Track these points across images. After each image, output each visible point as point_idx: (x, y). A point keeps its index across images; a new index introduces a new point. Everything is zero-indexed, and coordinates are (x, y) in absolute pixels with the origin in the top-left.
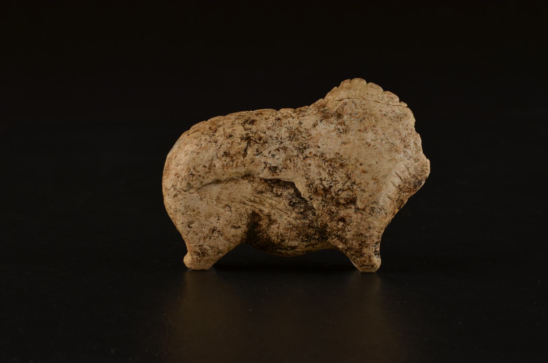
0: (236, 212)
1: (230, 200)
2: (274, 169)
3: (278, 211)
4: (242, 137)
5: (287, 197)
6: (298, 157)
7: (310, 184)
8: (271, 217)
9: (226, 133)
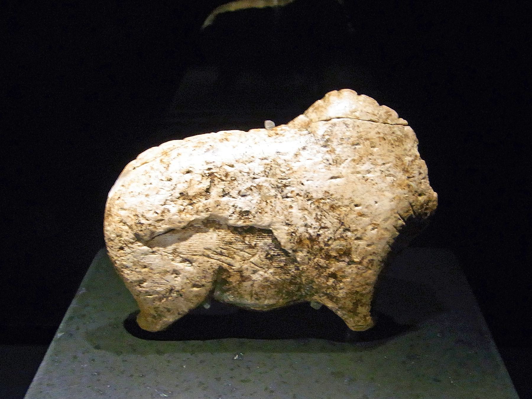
3: (252, 265)
7: (293, 232)
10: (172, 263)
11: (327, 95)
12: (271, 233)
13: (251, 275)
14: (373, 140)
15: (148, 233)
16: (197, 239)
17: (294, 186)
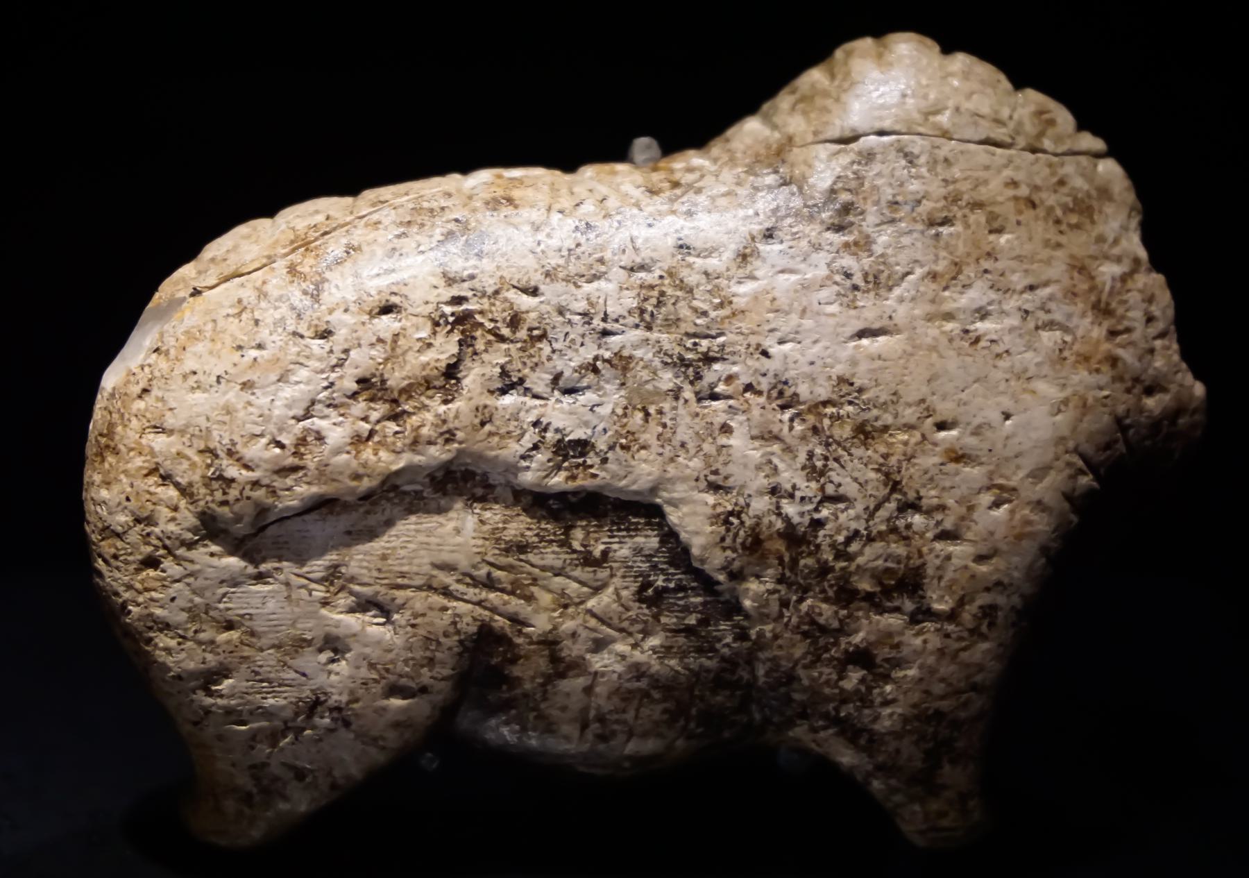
0: (409, 629)
1: (386, 581)
3: (593, 622)
4: (436, 316)
5: (628, 567)
6: (677, 398)
7: (731, 513)
8: (561, 650)
10: (324, 612)
13: (588, 656)
14: (997, 209)
17: (736, 358)
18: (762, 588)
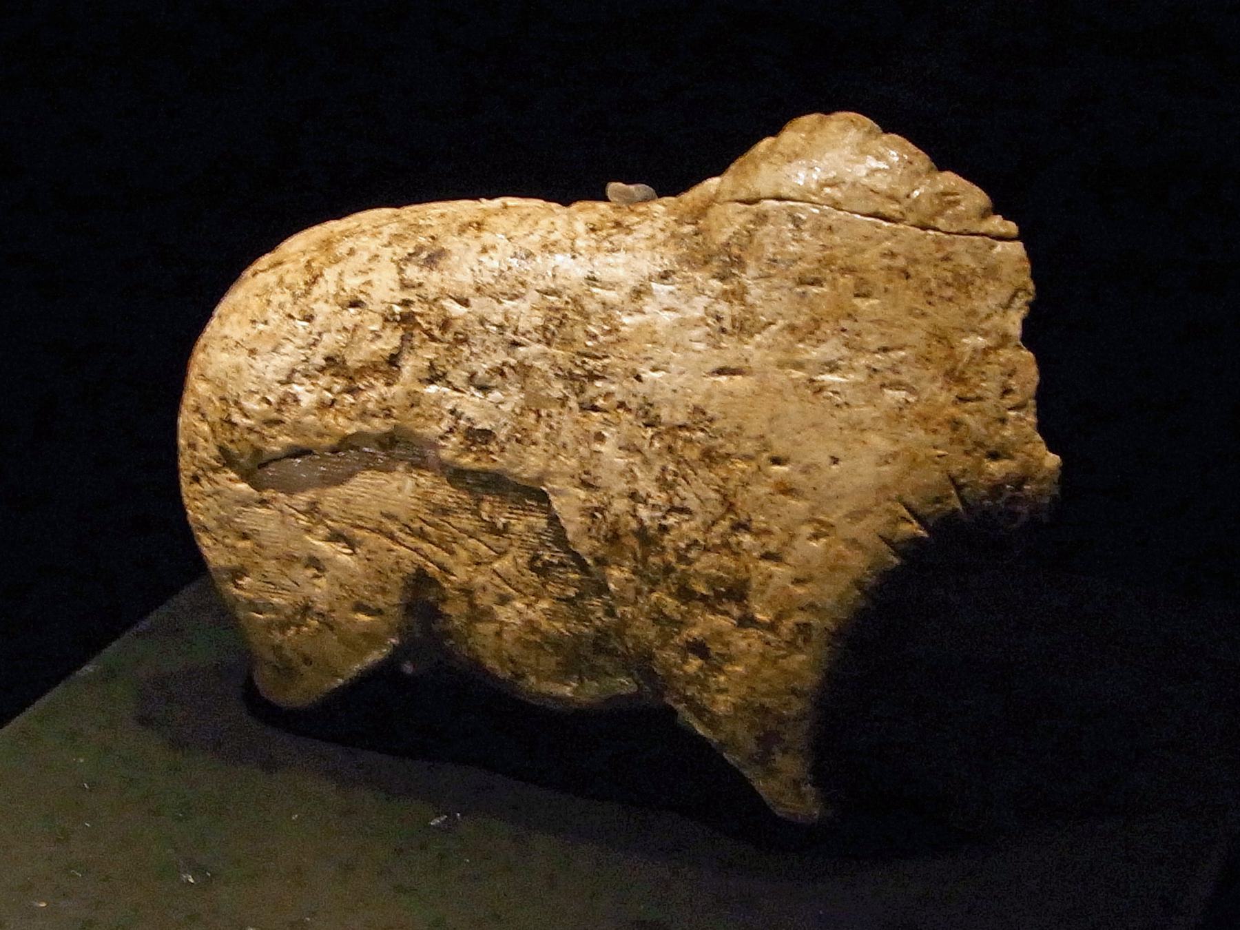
0: (366, 561)
1: (350, 521)
2: (478, 437)
3: (498, 581)
4: (387, 314)
7: (596, 509)
9: (343, 289)
10: (308, 537)
11: (839, 119)
12: (544, 502)
13: (495, 607)
14: (867, 276)
15: (249, 452)
16: (367, 486)
17: (615, 379)
18: (622, 576)
